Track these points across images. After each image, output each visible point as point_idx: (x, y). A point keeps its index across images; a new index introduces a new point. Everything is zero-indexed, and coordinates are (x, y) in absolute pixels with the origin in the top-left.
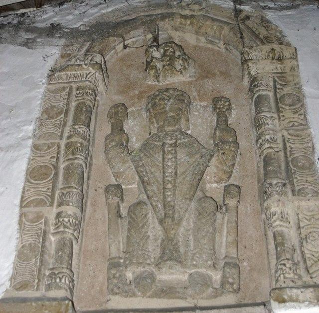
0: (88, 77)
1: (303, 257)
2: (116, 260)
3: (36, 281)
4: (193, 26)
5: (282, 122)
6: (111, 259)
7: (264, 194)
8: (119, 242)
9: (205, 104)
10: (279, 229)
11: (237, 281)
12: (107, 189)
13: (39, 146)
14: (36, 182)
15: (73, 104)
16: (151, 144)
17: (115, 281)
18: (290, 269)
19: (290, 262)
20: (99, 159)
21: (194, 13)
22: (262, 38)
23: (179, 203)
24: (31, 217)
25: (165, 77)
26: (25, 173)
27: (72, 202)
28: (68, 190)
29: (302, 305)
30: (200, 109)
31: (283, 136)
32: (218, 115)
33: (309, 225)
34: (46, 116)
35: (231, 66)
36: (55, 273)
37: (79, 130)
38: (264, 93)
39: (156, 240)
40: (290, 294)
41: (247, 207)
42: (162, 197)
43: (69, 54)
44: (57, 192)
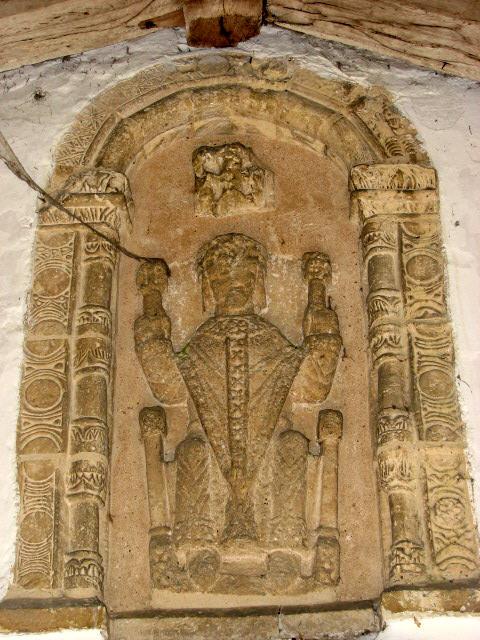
2: (162, 532)
3: (52, 573)
4: (270, 113)
5: (408, 308)
7: (378, 435)
8: (165, 502)
9: (289, 257)
10: (397, 491)
14: (38, 409)
15: (83, 266)
16: (208, 338)
18: (410, 556)
19: (411, 545)
20: (126, 360)
21: (274, 88)
22: (384, 145)
23: (252, 440)
24: (35, 469)
25: (226, 207)
28: (86, 424)
31: (409, 334)
32: (311, 286)
33: (440, 487)
34: (40, 289)
35: (332, 186)
37: (96, 316)
38: (383, 253)
39: (219, 502)
41: (354, 442)
43: (70, 167)
44: (71, 427)
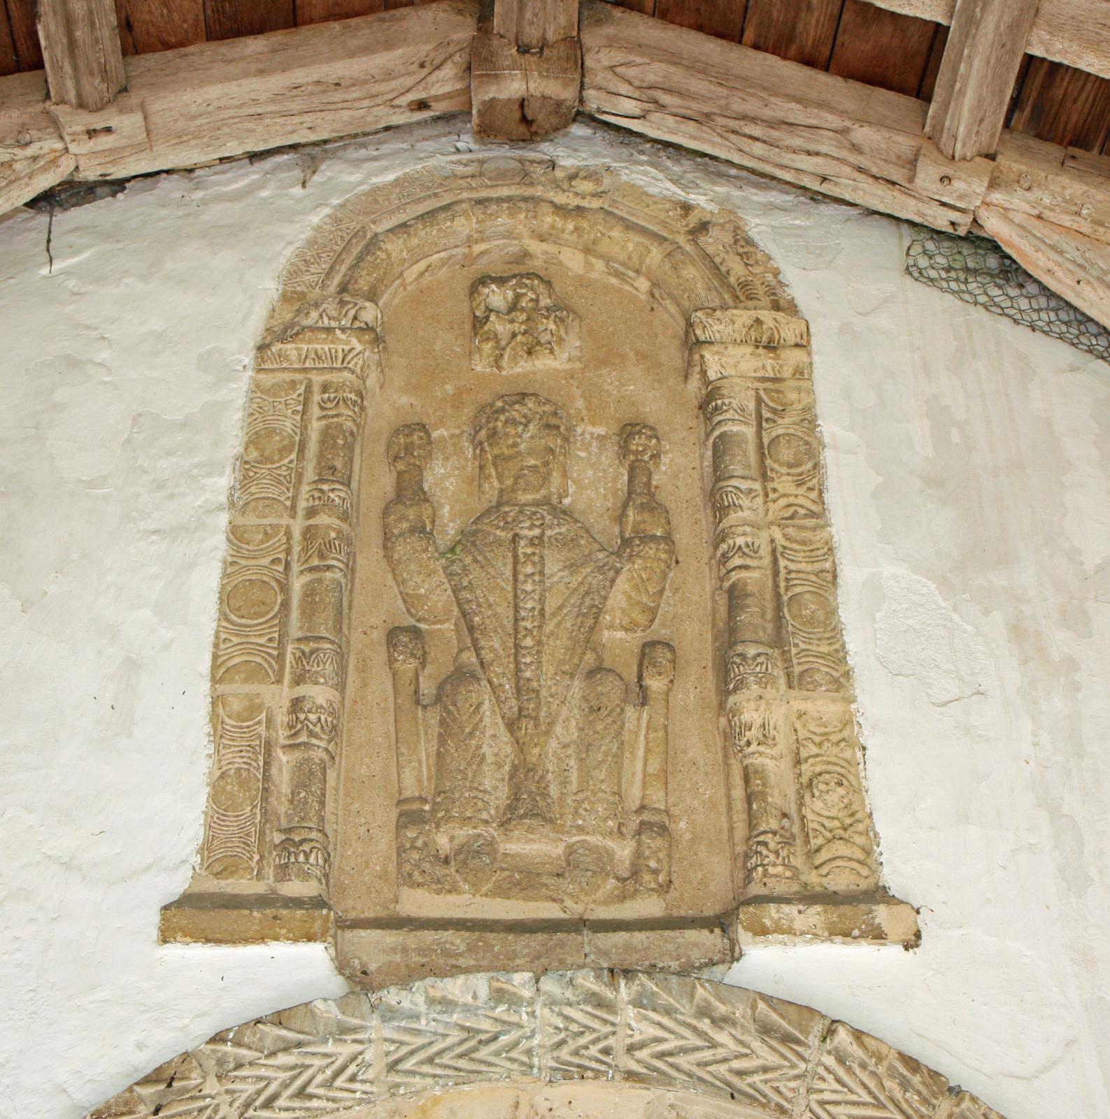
0: (348, 359)
1: (803, 830)
2: (415, 806)
3: (256, 857)
4: (579, 236)
6: (406, 801)
7: (726, 678)
8: (420, 761)
11: (665, 865)
12: (392, 636)
13: (244, 532)
14: (243, 621)
15: (316, 426)
16: (488, 534)
17: (415, 856)
20: (370, 561)
21: (584, 203)
24: (237, 706)
26: (217, 595)
27: (323, 676)
28: (313, 645)
29: (797, 939)
30: (590, 443)
31: (772, 541)
34: (254, 454)
35: (661, 338)
36: (293, 840)
37: (332, 495)
38: (735, 428)
40: (776, 916)
42: (512, 666)
